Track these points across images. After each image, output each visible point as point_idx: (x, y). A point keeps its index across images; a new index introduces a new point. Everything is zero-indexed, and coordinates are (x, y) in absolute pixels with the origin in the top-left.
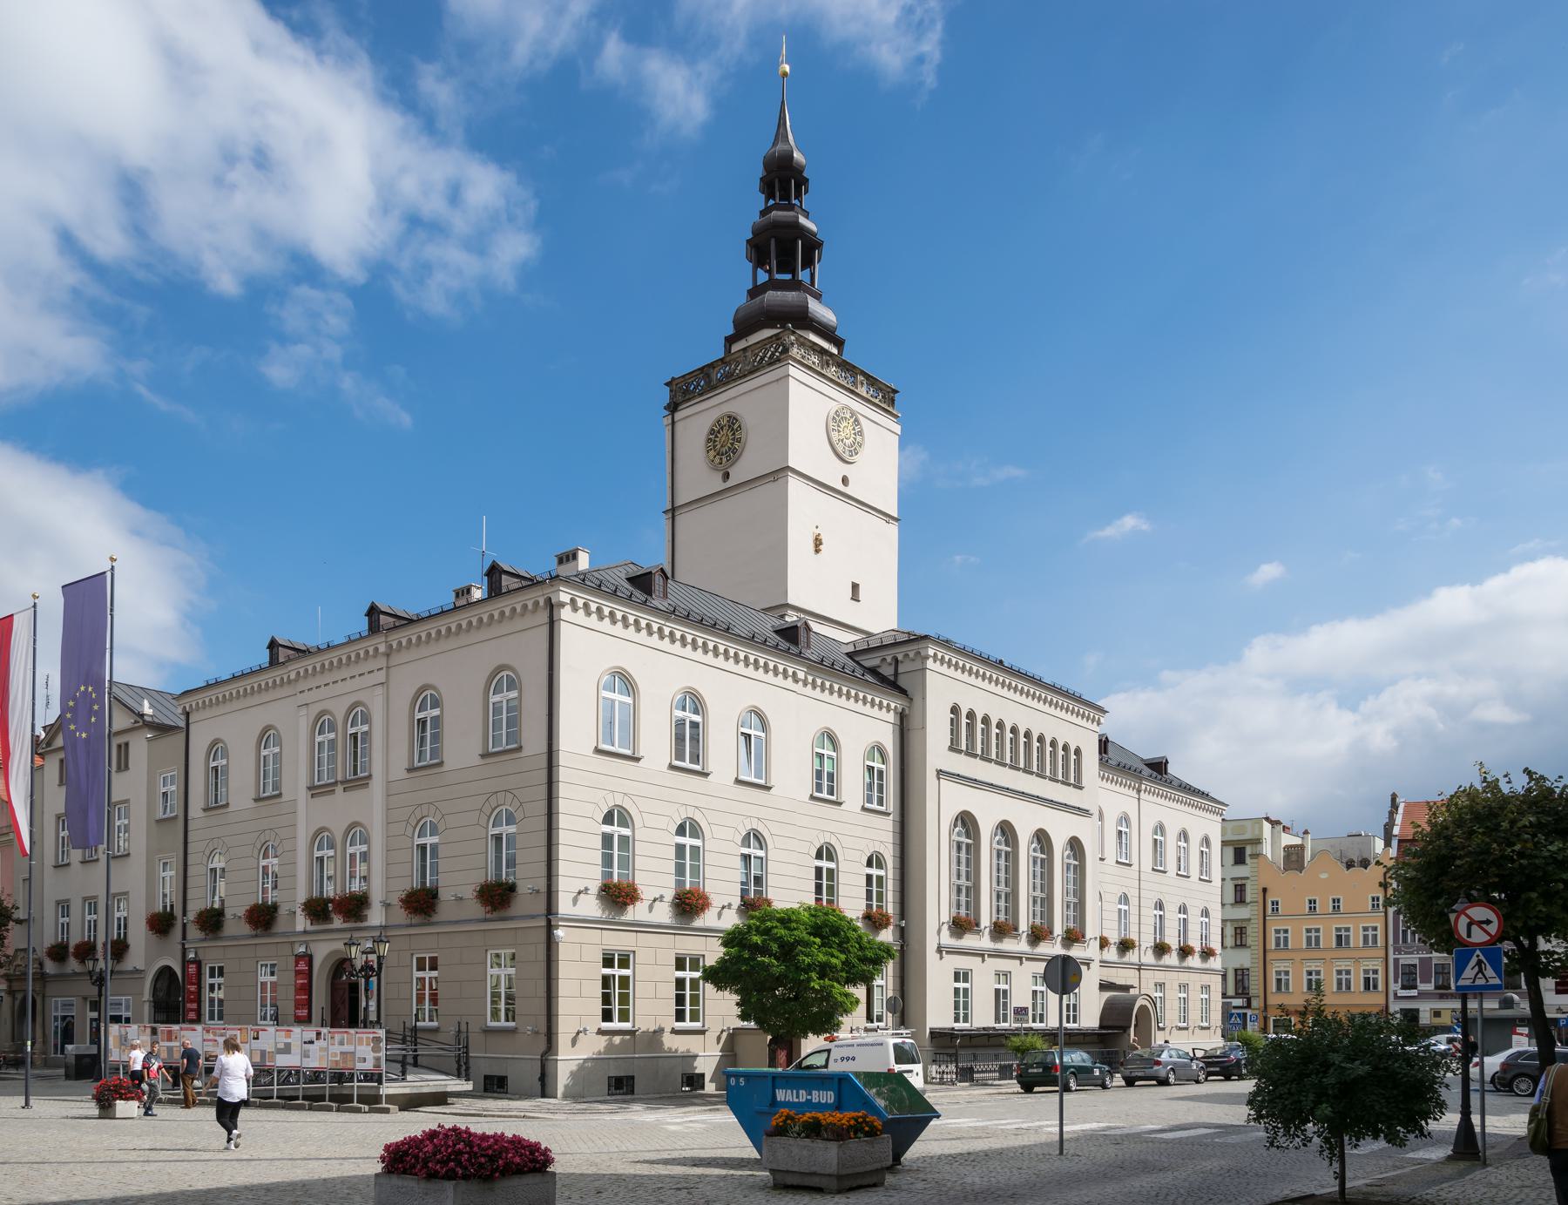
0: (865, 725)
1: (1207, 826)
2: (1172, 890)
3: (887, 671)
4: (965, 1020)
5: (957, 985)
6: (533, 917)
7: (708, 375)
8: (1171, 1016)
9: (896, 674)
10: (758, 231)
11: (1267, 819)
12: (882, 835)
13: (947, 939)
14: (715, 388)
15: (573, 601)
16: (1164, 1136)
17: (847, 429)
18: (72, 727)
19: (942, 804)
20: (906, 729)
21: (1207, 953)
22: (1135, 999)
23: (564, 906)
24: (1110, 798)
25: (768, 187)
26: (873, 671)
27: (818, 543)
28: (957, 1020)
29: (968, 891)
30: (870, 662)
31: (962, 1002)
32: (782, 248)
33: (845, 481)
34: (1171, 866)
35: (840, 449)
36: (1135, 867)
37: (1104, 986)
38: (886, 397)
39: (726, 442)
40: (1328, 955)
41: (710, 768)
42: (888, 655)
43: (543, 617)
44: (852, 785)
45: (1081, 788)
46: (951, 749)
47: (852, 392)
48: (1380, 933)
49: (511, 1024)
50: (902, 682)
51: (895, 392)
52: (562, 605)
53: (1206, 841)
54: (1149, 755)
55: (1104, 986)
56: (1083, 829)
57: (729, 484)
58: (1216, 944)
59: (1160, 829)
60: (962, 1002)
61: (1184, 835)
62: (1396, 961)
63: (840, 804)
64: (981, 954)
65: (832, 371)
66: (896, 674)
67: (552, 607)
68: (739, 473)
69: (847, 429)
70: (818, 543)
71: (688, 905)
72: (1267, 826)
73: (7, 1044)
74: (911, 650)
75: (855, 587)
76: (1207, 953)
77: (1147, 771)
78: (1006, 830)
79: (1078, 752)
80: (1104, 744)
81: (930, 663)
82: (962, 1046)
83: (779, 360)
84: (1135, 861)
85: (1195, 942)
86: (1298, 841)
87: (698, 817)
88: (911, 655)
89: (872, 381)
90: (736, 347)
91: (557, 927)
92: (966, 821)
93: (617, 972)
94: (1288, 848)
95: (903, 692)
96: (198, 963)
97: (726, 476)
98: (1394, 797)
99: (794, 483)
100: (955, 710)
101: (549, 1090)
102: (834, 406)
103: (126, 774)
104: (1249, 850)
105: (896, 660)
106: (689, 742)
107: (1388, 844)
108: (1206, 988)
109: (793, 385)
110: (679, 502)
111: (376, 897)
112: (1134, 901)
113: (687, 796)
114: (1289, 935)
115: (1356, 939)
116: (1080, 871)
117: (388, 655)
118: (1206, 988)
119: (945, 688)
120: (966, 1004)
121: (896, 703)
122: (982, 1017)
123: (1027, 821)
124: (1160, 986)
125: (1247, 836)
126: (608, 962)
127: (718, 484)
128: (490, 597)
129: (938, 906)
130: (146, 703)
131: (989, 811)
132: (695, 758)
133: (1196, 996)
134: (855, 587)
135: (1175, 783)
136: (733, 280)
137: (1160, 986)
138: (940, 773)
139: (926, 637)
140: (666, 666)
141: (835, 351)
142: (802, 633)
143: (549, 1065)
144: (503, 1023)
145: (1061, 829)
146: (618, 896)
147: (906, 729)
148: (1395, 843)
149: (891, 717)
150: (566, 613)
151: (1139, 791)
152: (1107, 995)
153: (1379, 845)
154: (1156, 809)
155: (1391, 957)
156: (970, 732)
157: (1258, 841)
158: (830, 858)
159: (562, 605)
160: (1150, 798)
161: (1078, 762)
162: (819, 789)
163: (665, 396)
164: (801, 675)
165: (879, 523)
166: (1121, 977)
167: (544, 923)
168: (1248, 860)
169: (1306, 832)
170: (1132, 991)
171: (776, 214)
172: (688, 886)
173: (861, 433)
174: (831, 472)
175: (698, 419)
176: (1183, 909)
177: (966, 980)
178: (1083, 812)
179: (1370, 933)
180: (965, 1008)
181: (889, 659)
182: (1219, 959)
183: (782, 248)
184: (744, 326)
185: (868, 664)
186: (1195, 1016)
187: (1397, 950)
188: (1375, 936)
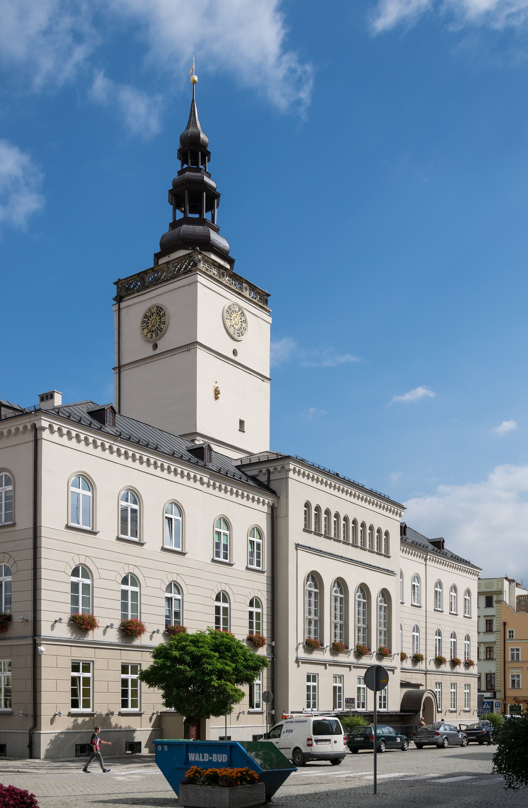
0: (248, 514)
1: (469, 583)
2: (447, 623)
3: (263, 479)
5: (309, 684)
6: (23, 638)
8: (446, 704)
9: (269, 480)
10: (176, 185)
11: (506, 578)
12: (259, 585)
13: (302, 654)
14: (147, 287)
15: (51, 427)
17: (236, 319)
19: (299, 566)
20: (275, 517)
21: (468, 664)
22: (423, 693)
24: (407, 563)
25: (183, 155)
26: (254, 478)
27: (217, 393)
32: (192, 196)
33: (235, 352)
34: (446, 607)
35: (231, 331)
36: (423, 608)
37: (404, 685)
38: (262, 299)
39: (155, 323)
41: (145, 540)
43: (30, 437)
45: (389, 557)
46: (305, 530)
47: (240, 294)
50: (273, 486)
52: (43, 429)
54: (432, 536)
55: (404, 685)
56: (391, 584)
57: (157, 351)
58: (474, 658)
61: (454, 588)
63: (231, 565)
65: (226, 280)
67: (36, 430)
69: (236, 319)
70: (217, 393)
71: (130, 631)
72: (506, 583)
74: (278, 465)
75: (242, 423)
76: (468, 664)
77: (431, 547)
79: (387, 534)
80: (404, 529)
81: (291, 474)
83: (190, 271)
84: (423, 604)
88: (279, 468)
89: (253, 288)
90: (162, 261)
91: (40, 645)
92: (315, 578)
93: (82, 675)
94: (519, 597)
97: (155, 346)
99: (201, 353)
100: (307, 505)
101: (35, 754)
102: (228, 303)
104: (495, 598)
105: (269, 472)
106: (130, 523)
112: (422, 630)
113: (129, 558)
114: (520, 652)
116: (388, 610)
118: (468, 686)
119: (301, 491)
123: (354, 577)
127: (148, 351)
129: (296, 632)
132: (135, 533)
133: (461, 691)
134: (242, 423)
135: (449, 555)
136: (161, 217)
137: (439, 684)
138: (297, 546)
140: (115, 472)
141: (228, 266)
142: (206, 452)
143: (35, 737)
146: (82, 624)
147: (275, 517)
149: (265, 509)
151: (426, 560)
152: (405, 690)
154: (436, 571)
156: (316, 519)
157: (500, 593)
158: (225, 600)
159: (43, 429)
160: (433, 564)
164: (206, 480)
165: (257, 381)
166: (414, 678)
167: (31, 642)
168: (494, 604)
170: (421, 688)
173: (245, 321)
174: (225, 346)
175: (137, 308)
178: (390, 573)
181: (264, 471)
183: (192, 196)
184: (167, 247)
185: (250, 473)
186: (461, 703)
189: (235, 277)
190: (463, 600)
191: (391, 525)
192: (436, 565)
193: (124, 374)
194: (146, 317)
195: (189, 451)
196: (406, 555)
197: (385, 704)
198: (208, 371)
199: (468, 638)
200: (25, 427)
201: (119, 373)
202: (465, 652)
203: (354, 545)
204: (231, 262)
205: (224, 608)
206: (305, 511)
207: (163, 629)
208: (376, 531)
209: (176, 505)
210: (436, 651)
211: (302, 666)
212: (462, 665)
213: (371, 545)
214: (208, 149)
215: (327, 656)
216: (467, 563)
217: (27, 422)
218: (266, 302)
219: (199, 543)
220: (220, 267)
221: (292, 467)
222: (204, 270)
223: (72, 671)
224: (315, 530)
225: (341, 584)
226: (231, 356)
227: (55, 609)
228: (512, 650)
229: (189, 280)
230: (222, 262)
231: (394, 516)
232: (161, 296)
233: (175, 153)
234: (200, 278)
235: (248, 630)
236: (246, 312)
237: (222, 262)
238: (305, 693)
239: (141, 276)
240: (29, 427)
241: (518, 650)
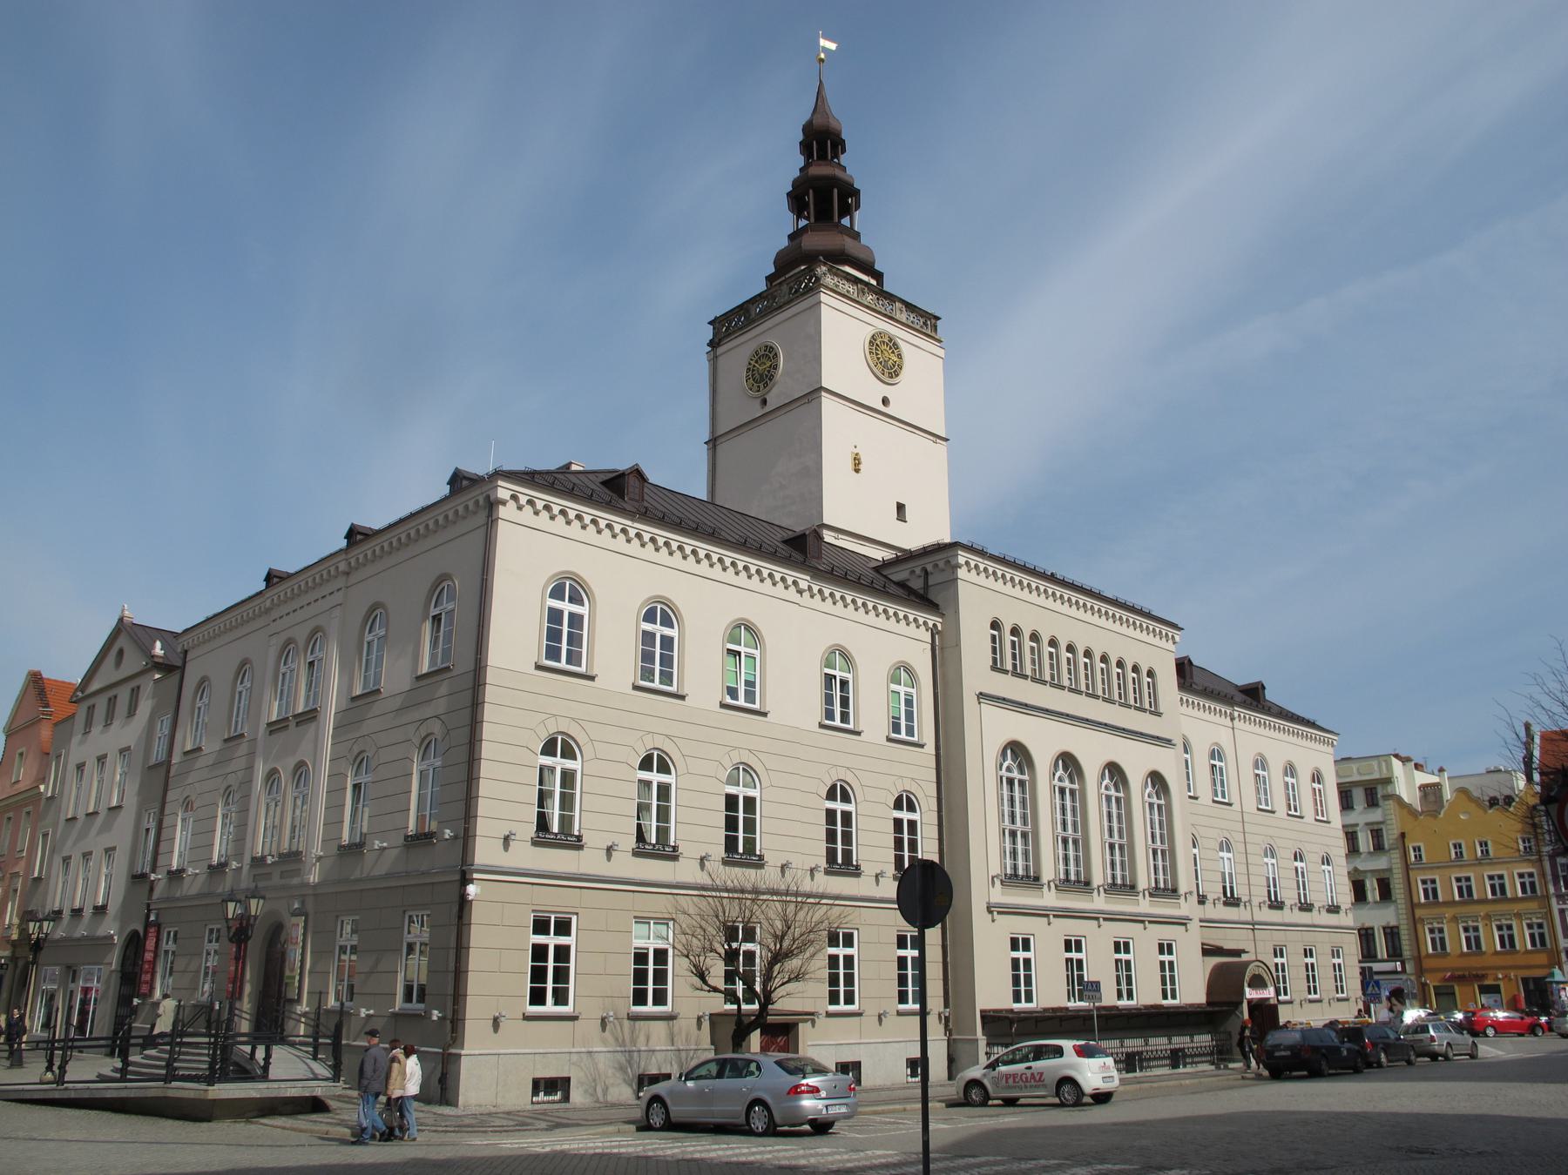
0: (888, 641)
1: (1316, 756)
2: (1286, 834)
3: (916, 584)
5: (1015, 954)
7: (748, 311)
8: (1296, 984)
9: (926, 586)
10: (797, 184)
11: (1396, 756)
14: (754, 321)
19: (987, 732)
20: (944, 652)
22: (1247, 964)
23: (485, 851)
24: (1204, 725)
25: (806, 147)
26: (902, 585)
28: (1017, 999)
29: (1021, 836)
30: (899, 574)
31: (1021, 975)
32: (823, 196)
33: (885, 401)
34: (1279, 804)
36: (1236, 807)
37: (1208, 951)
38: (926, 322)
39: (762, 373)
40: (1516, 908)
42: (917, 565)
43: (481, 518)
44: (873, 707)
45: (1159, 714)
46: (994, 668)
47: (891, 318)
50: (931, 596)
51: (937, 318)
53: (1317, 777)
54: (1241, 681)
55: (1208, 951)
56: (1167, 762)
57: (768, 408)
59: (1260, 763)
60: (1021, 975)
61: (1290, 770)
65: (869, 298)
67: (492, 505)
72: (1396, 763)
74: (939, 558)
75: (901, 508)
77: (1239, 697)
78: (1114, 771)
79: (1150, 674)
80: (1184, 669)
81: (962, 573)
83: (811, 289)
84: (1235, 799)
86: (1434, 779)
87: (668, 747)
88: (941, 564)
89: (910, 307)
91: (471, 881)
92: (1017, 751)
93: (551, 941)
94: (1423, 788)
96: (158, 926)
97: (764, 402)
99: (827, 402)
100: (995, 625)
102: (870, 331)
104: (1380, 792)
105: (926, 573)
106: (657, 660)
107: (1529, 778)
112: (1238, 847)
113: (655, 722)
114: (1438, 884)
115: (1515, 889)
116: (1166, 811)
117: (348, 574)
119: (981, 597)
122: (1051, 992)
123: (1094, 751)
125: (1376, 776)
126: (541, 926)
130: (158, 644)
132: (667, 677)
133: (1323, 962)
134: (901, 508)
135: (1274, 710)
137: (1279, 952)
138: (981, 696)
140: (626, 569)
141: (874, 282)
142: (811, 540)
145: (1137, 760)
147: (944, 652)
150: (503, 512)
151: (1232, 719)
152: (1214, 961)
153: (1521, 783)
154: (1249, 737)
156: (1012, 649)
157: (1388, 781)
158: (846, 798)
159: (504, 503)
160: (1247, 726)
161: (1153, 687)
162: (829, 715)
163: (708, 333)
164: (803, 585)
166: (1229, 940)
168: (1381, 802)
169: (1441, 770)
170: (1244, 957)
171: (815, 170)
175: (740, 351)
181: (918, 571)
183: (823, 196)
184: (785, 262)
185: (895, 578)
186: (1326, 983)
189: (881, 293)
190: (1208, 769)
191: (1159, 656)
192: (1251, 728)
193: (722, 448)
195: (785, 542)
196: (1189, 711)
197: (1173, 991)
198: (839, 428)
200: (477, 502)
203: (1018, 673)
204: (878, 276)
205: (843, 813)
206: (993, 637)
208: (1114, 664)
209: (747, 628)
211: (1002, 920)
215: (1049, 898)
216: (1311, 724)
219: (793, 697)
220: (856, 281)
222: (831, 286)
223: (535, 933)
224: (1014, 666)
228: (1424, 882)
230: (865, 278)
231: (1163, 643)
232: (771, 332)
234: (823, 297)
236: (900, 343)
237: (865, 278)
238: (1009, 973)
239: (743, 309)
240: (481, 502)
241: (1501, 877)
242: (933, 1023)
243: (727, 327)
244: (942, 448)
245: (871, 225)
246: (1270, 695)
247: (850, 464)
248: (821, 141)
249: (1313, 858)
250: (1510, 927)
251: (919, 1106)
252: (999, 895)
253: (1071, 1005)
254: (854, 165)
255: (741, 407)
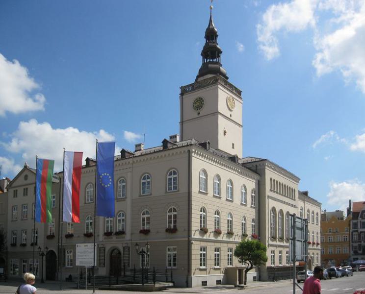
4: (231, 265)
6: (184, 237)
9: (256, 169)
12: (251, 214)
16: (167, 284)
18: (108, 175)
19: (270, 204)
20: (260, 185)
21: (318, 244)
27: (225, 133)
29: (274, 229)
32: (211, 52)
33: (231, 116)
38: (239, 93)
39: (199, 104)
48: (348, 238)
49: (72, 267)
50: (258, 171)
58: (319, 242)
62: (352, 245)
64: (276, 246)
66: (256, 169)
68: (203, 112)
70: (225, 133)
71: (230, 234)
73: (286, 285)
76: (318, 244)
79: (294, 190)
81: (266, 167)
82: (276, 271)
85: (315, 242)
89: (236, 89)
90: (200, 79)
92: (274, 210)
95: (259, 174)
97: (199, 113)
98: (350, 201)
99: (220, 116)
100: (271, 179)
101: (189, 285)
103: (16, 198)
105: (256, 166)
108: (317, 254)
109: (219, 90)
110: (184, 120)
111: (128, 231)
118: (317, 254)
120: (218, 259)
121: (257, 177)
124: (313, 254)
127: (195, 115)
128: (180, 141)
129: (268, 234)
131: (279, 207)
134: (233, 148)
136: (198, 62)
138: (268, 197)
139: (265, 160)
143: (189, 279)
144: (70, 266)
146: (204, 231)
147: (260, 185)
148: (351, 214)
155: (351, 244)
163: (179, 91)
167: (187, 239)
172: (109, 231)
173: (234, 103)
174: (227, 113)
176: (313, 233)
177: (204, 251)
179: (345, 238)
180: (204, 261)
182: (143, 248)
183: (211, 52)
186: (211, 261)
187: (353, 242)
188: (347, 239)
194: (195, 103)
198: (222, 123)
199: (317, 233)
200: (184, 151)
201: (182, 124)
202: (215, 223)
207: (199, 229)
210: (215, 225)
212: (311, 245)
213: (280, 191)
214: (217, 34)
217: (186, 149)
218: (240, 94)
221: (194, 150)
225: (281, 212)
226: (229, 117)
227: (196, 225)
229: (213, 87)
233: (204, 35)
234: (219, 86)
235: (227, 228)
242: (96, 247)
243: (184, 91)
244: (241, 129)
245: (226, 65)
246: (309, 195)
247: (223, 134)
248: (211, 35)
249: (315, 233)
250: (340, 248)
251: (292, 291)
252: (271, 243)
253: (287, 265)
254: (220, 44)
255: (191, 113)
